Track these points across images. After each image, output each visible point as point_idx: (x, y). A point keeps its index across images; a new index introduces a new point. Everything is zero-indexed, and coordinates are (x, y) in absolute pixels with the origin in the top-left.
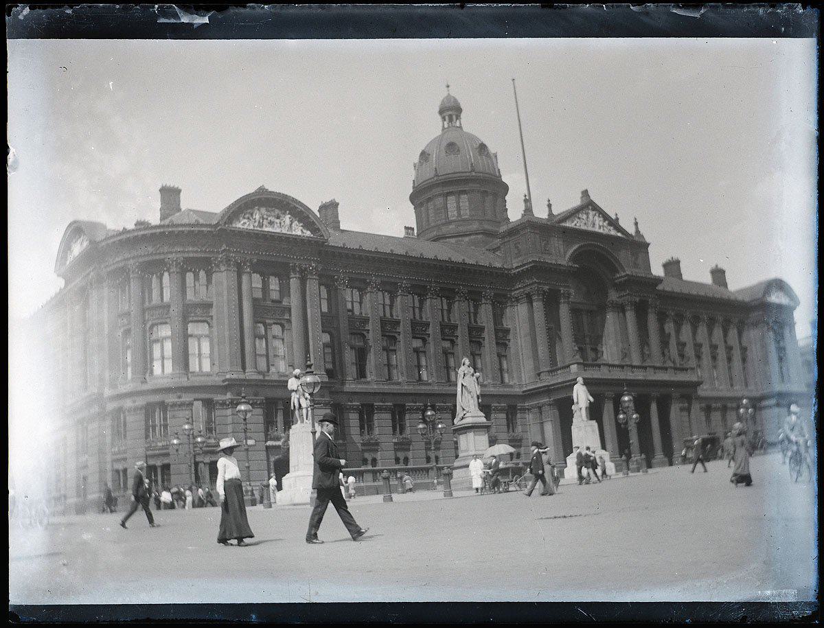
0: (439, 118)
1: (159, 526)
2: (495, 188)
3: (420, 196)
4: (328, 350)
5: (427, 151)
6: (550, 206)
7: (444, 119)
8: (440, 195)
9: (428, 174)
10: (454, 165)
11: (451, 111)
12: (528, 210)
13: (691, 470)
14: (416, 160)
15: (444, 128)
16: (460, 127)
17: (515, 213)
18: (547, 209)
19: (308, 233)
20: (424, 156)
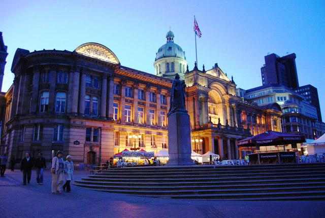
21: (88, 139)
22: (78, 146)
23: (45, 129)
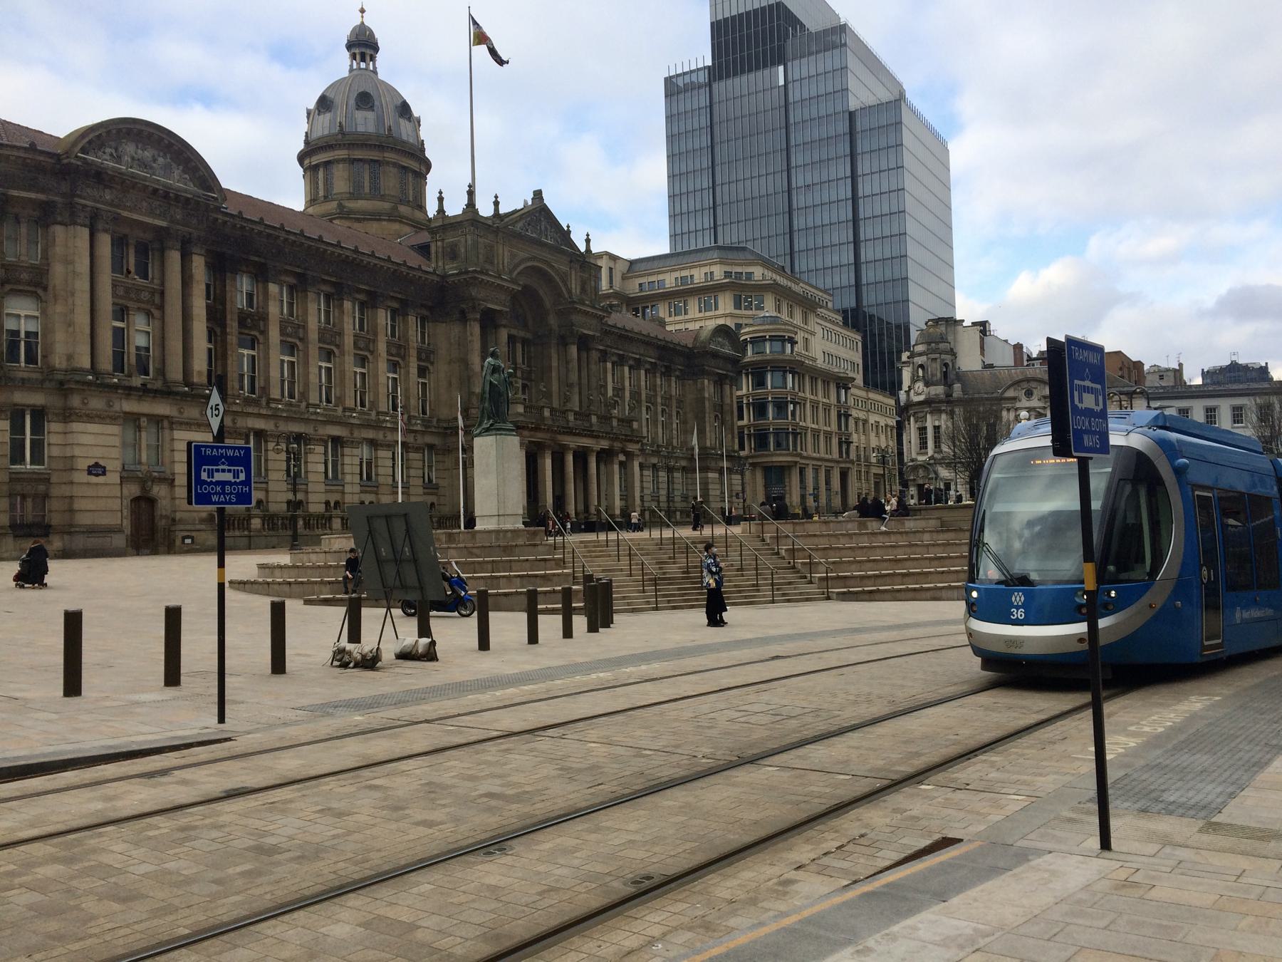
0: (347, 54)
1: (1181, 365)
2: (415, 163)
3: (314, 156)
4: (1168, 382)
5: (331, 95)
6: (496, 204)
7: (354, 57)
8: (343, 160)
9: (325, 125)
10: (365, 122)
11: (363, 45)
12: (471, 204)
13: (1095, 842)
14: (312, 106)
15: (351, 70)
16: (375, 72)
17: (432, 210)
18: (493, 207)
19: (191, 187)
20: (324, 103)
22: (101, 479)
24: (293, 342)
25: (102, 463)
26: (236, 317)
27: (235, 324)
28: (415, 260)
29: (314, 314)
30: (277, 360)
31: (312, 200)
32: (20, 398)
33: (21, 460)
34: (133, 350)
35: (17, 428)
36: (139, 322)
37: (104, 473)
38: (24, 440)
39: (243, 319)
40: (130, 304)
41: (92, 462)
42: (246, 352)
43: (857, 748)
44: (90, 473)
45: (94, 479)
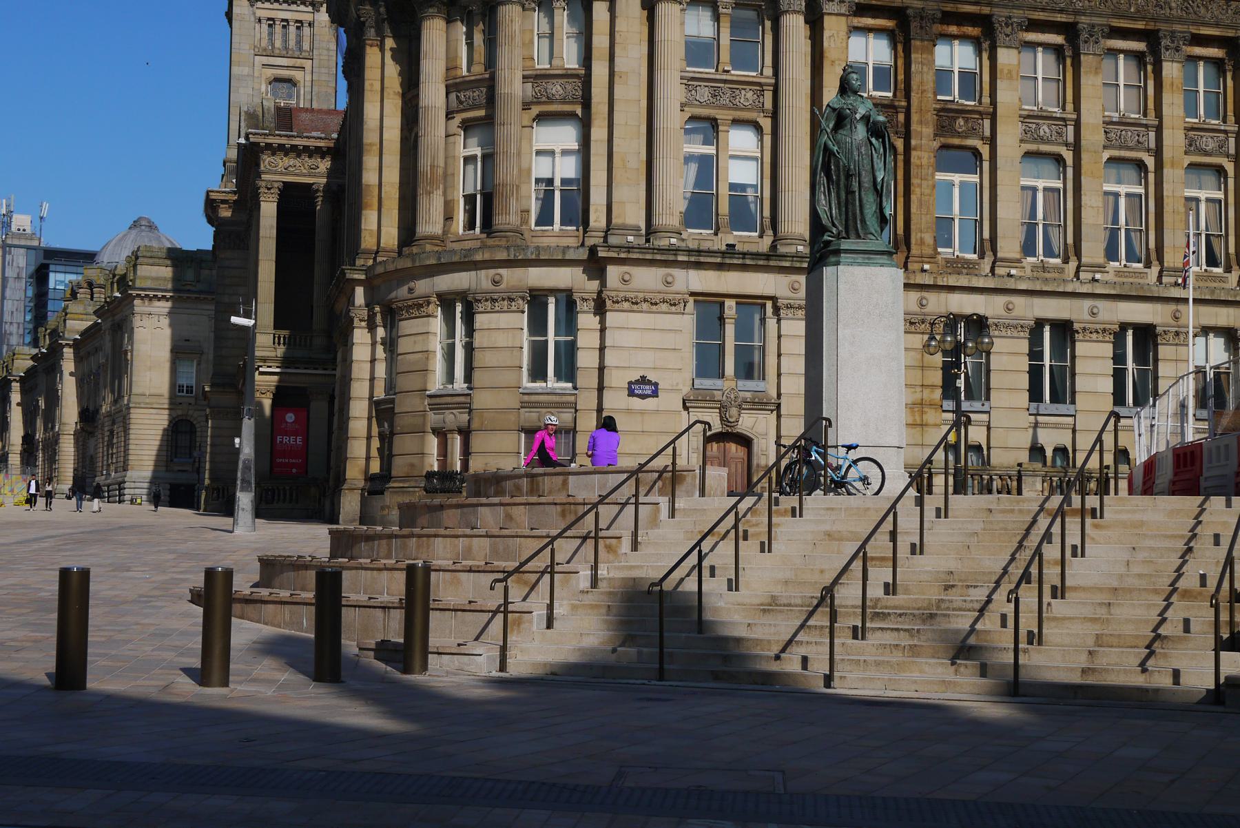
21: (709, 362)
22: (650, 403)
23: (480, 320)
24: (1057, 147)
25: (651, 377)
26: (931, 117)
27: (928, 131)
28: (412, 284)
29: (1110, 87)
30: (1021, 184)
31: (354, 290)
32: (539, 277)
33: (544, 377)
34: (724, 192)
35: (538, 325)
36: (741, 140)
37: (655, 394)
38: (722, 348)
39: (946, 117)
40: (720, 115)
41: (635, 376)
42: (957, 178)
43: (968, 587)
44: (631, 393)
45: (636, 403)
